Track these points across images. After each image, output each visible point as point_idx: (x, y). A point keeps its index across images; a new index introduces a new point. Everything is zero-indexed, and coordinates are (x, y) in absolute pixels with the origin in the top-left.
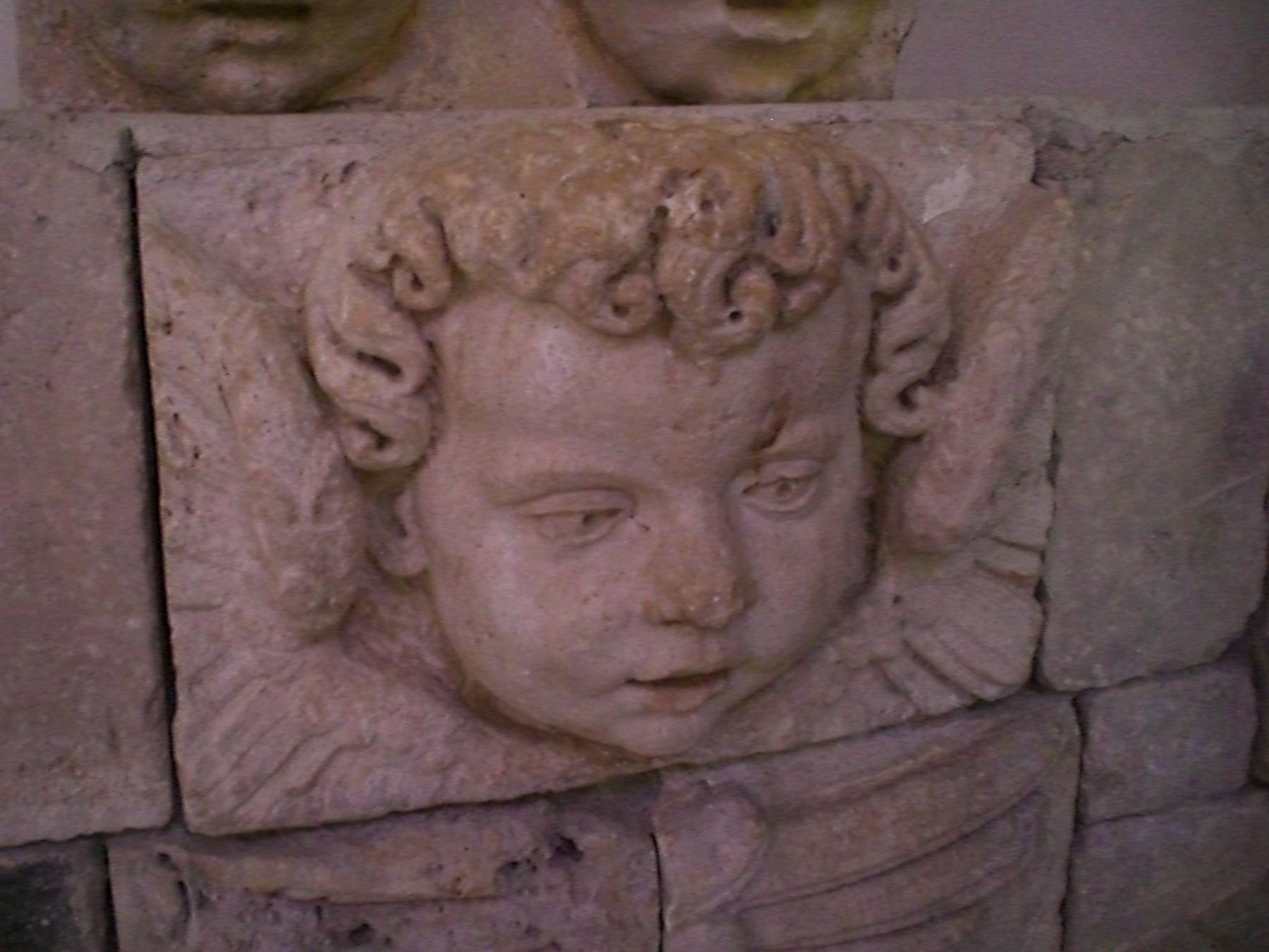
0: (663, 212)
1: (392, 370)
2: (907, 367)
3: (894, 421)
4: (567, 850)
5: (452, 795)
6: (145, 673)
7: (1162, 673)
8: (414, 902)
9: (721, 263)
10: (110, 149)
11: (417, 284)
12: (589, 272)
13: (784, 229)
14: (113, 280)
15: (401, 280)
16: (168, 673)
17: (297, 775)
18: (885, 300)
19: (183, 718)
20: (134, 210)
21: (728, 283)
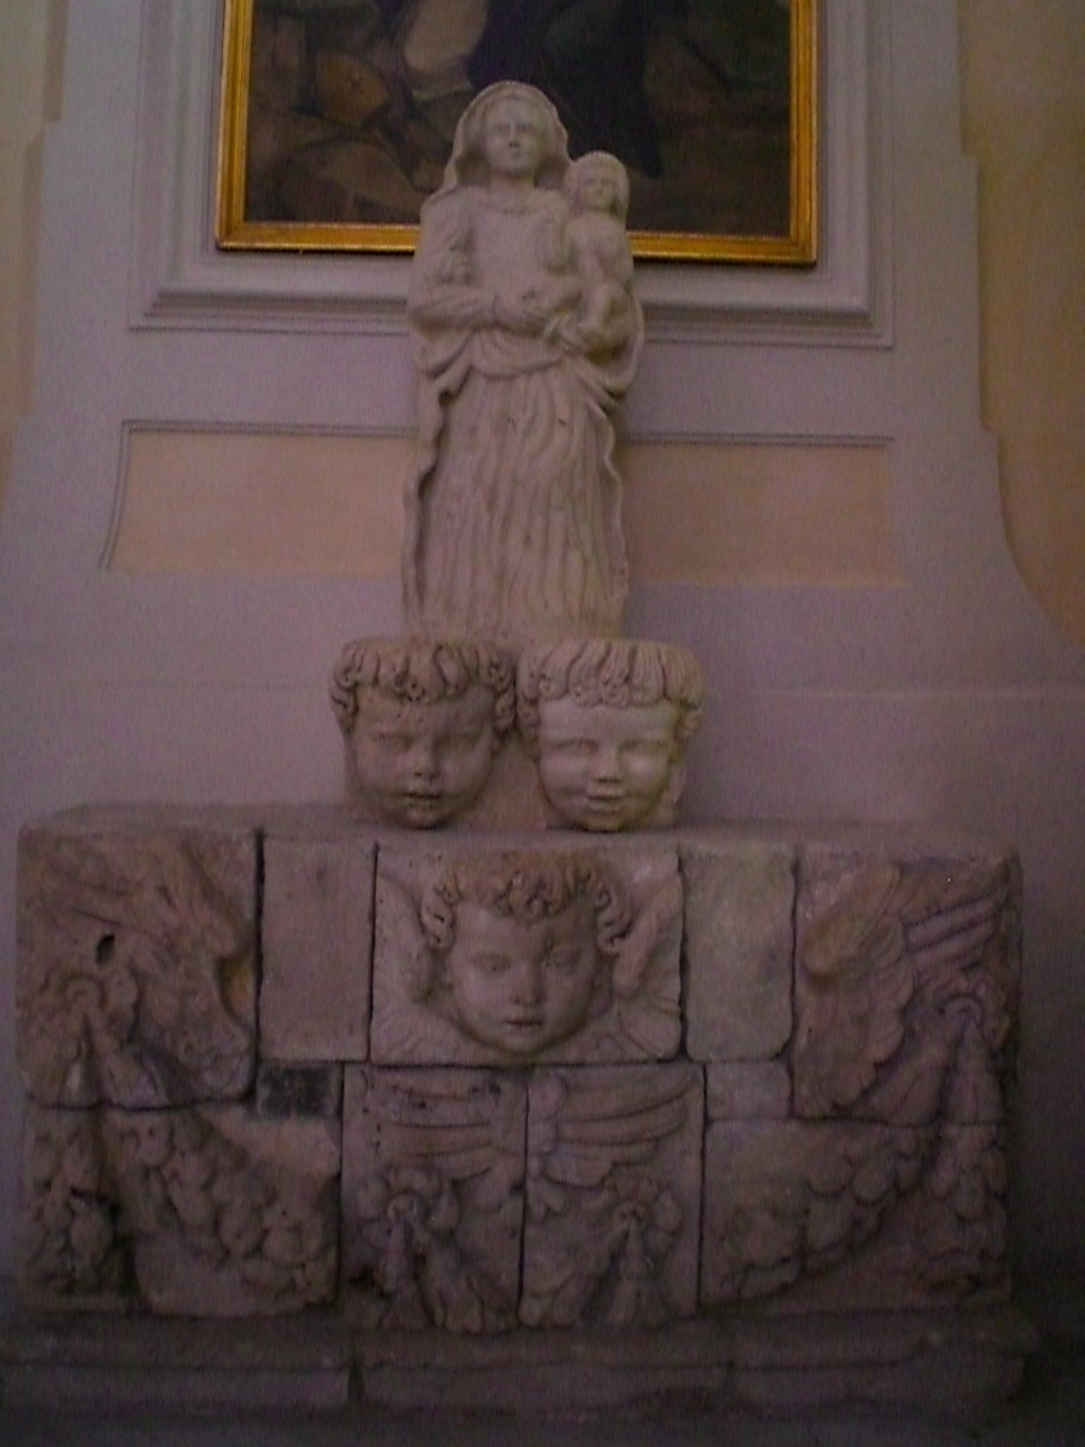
0: (511, 883)
1: (442, 920)
2: (608, 932)
3: (609, 949)
4: (496, 1090)
5: (457, 1060)
6: (364, 1007)
7: (742, 1060)
8: (441, 1097)
9: (526, 898)
10: (369, 848)
11: (450, 895)
12: (490, 898)
13: (548, 887)
14: (367, 886)
15: (446, 896)
16: (371, 1007)
17: (407, 1046)
18: (598, 910)
19: (373, 1023)
20: (301, 251)
21: (529, 902)
